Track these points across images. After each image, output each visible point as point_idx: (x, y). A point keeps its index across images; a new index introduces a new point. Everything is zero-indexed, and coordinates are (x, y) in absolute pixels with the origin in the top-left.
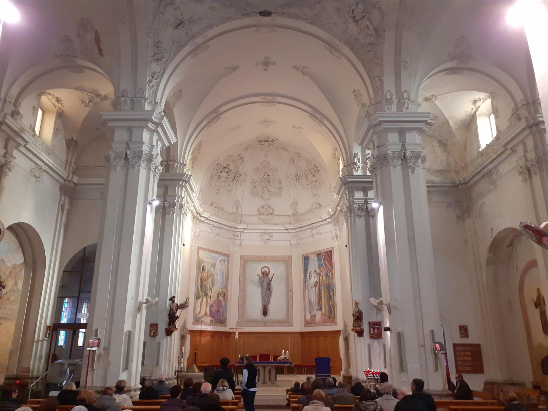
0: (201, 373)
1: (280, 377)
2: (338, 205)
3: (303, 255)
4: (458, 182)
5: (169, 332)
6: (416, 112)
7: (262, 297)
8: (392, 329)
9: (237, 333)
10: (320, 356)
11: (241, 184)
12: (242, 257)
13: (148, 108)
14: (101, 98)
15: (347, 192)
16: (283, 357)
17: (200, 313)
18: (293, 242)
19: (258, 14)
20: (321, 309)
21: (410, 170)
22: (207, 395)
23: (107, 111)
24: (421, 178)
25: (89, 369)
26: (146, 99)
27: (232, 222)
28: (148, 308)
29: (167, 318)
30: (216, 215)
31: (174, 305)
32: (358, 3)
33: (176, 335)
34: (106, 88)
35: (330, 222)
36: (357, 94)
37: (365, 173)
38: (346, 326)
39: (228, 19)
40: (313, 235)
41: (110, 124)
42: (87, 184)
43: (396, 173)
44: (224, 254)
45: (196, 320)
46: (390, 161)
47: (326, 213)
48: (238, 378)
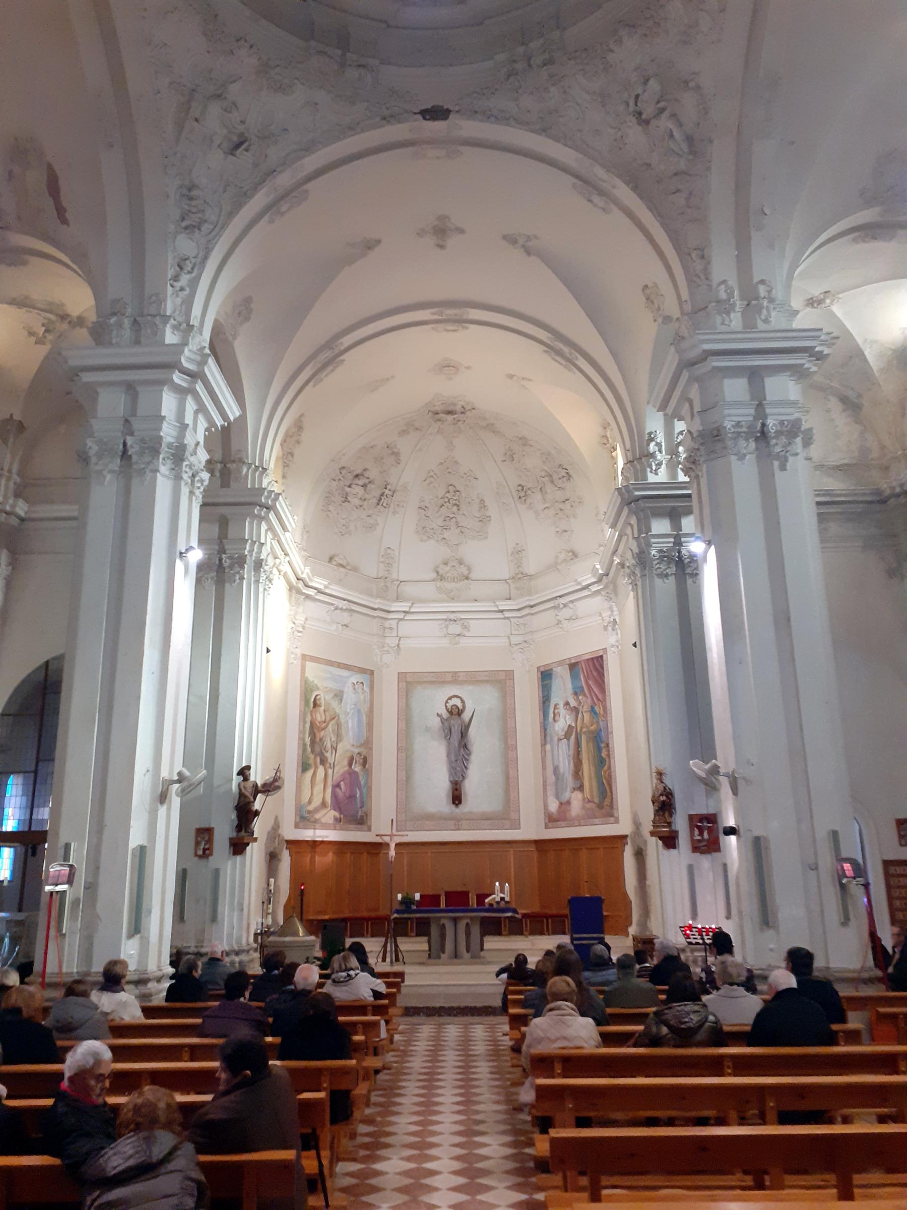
0: (313, 938)
1: (491, 943)
2: (615, 552)
3: (538, 668)
4: (888, 492)
5: (238, 847)
6: (789, 328)
7: (450, 762)
8: (742, 831)
9: (393, 846)
10: (582, 895)
11: (395, 513)
12: (402, 676)
13: (171, 337)
14: (70, 322)
15: (633, 521)
16: (497, 897)
17: (310, 802)
18: (515, 640)
19: (420, 117)
20: (581, 788)
21: (776, 464)
22: (310, 992)
23: (82, 351)
24: (801, 484)
25: (52, 932)
26: (166, 319)
27: (377, 597)
28: (183, 793)
29: (234, 816)
30: (340, 582)
31: (249, 784)
32: (648, 80)
33: (255, 852)
34: (79, 299)
35: (597, 592)
36: (650, 294)
37: (674, 475)
38: (637, 825)
39: (353, 128)
40: (559, 622)
41: (87, 377)
42: (49, 519)
43: (743, 470)
44: (362, 671)
45: (303, 818)
46: (729, 443)
47: (586, 572)
48: (396, 946)
